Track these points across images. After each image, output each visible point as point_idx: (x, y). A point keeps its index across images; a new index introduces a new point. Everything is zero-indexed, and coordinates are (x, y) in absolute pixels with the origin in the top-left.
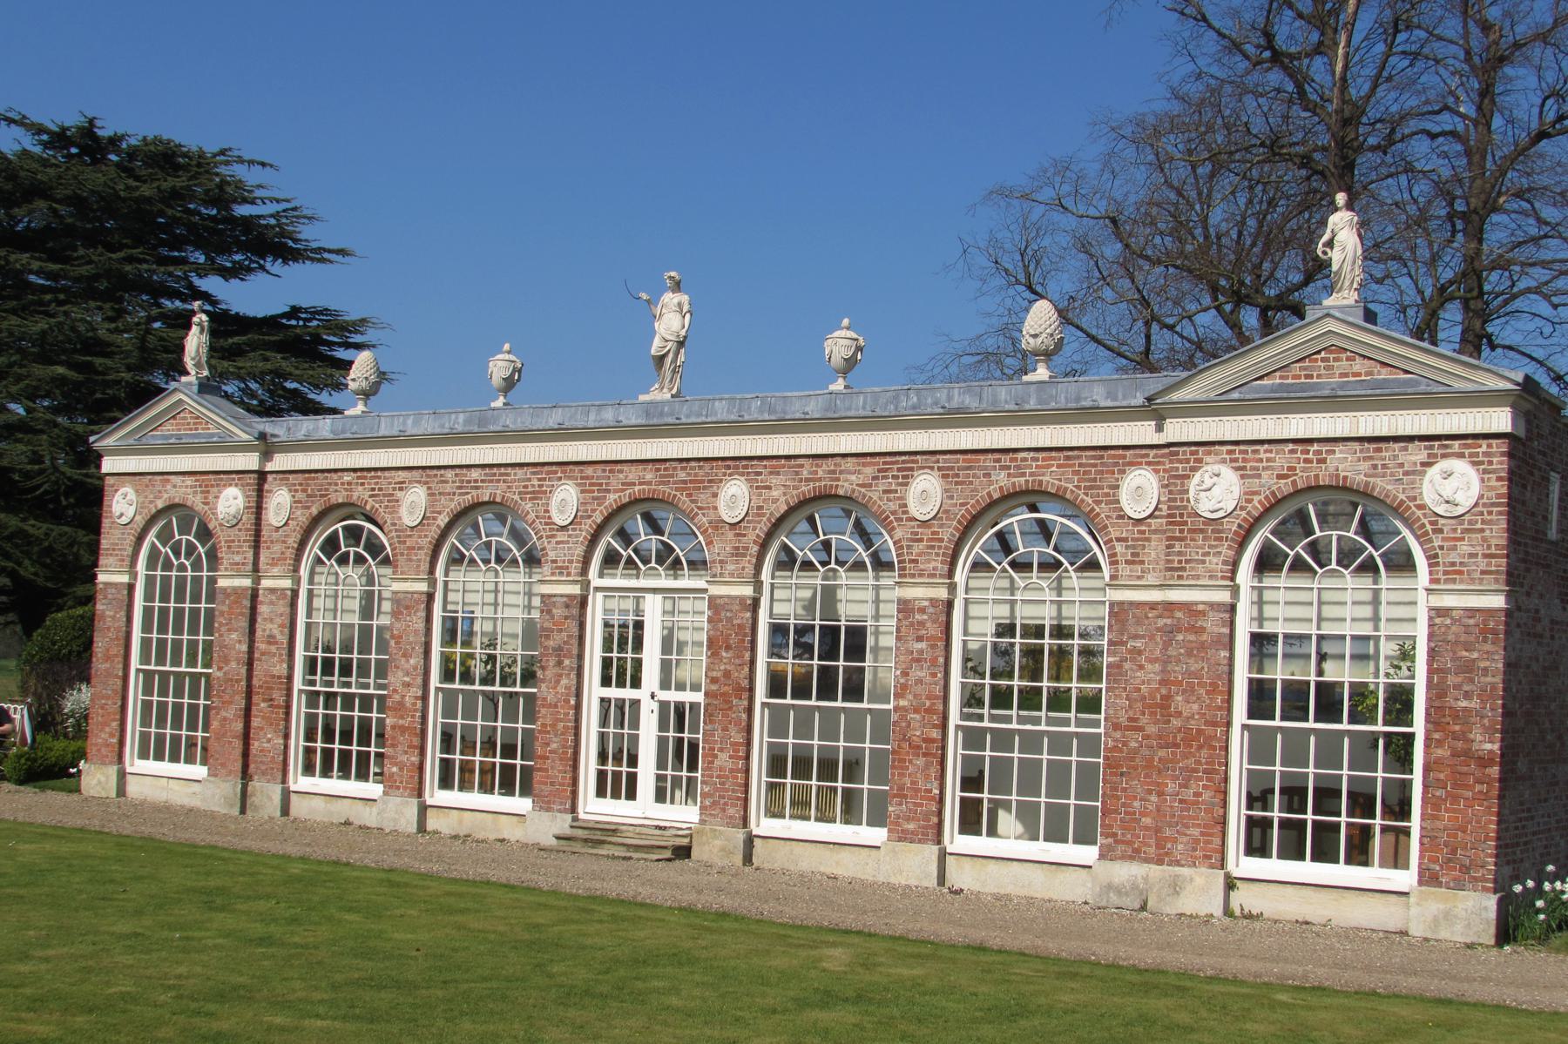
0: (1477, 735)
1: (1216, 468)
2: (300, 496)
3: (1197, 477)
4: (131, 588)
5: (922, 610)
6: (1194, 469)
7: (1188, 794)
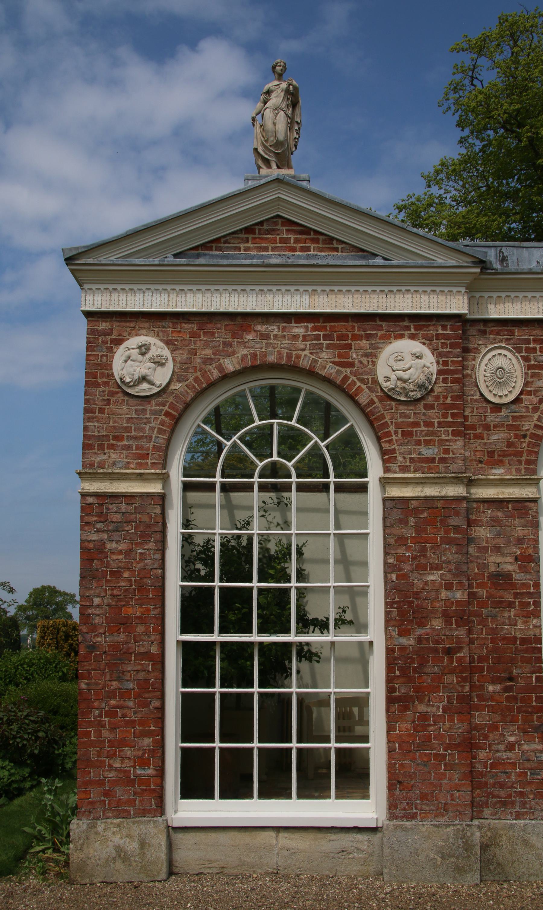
4: (162, 499)
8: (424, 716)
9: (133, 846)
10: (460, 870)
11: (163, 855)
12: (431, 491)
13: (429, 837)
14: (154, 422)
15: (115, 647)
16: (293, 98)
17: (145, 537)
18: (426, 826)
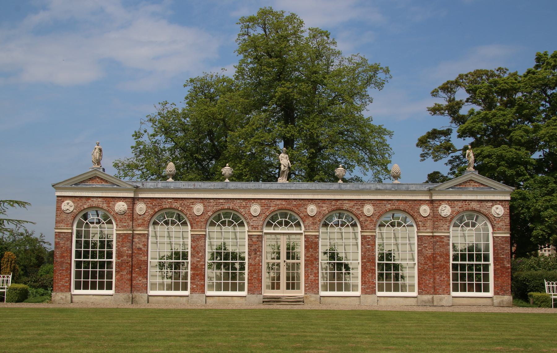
0: (505, 263)
1: (446, 205)
2: (150, 205)
3: (440, 208)
4: (72, 233)
5: (369, 238)
6: (440, 206)
7: (442, 279)
8: (122, 275)
9: (64, 297)
10: (128, 302)
11: (70, 299)
12: (125, 232)
13: (122, 296)
14: (70, 218)
15: (61, 261)
16: (100, 150)
17: (68, 240)
18: (121, 294)
